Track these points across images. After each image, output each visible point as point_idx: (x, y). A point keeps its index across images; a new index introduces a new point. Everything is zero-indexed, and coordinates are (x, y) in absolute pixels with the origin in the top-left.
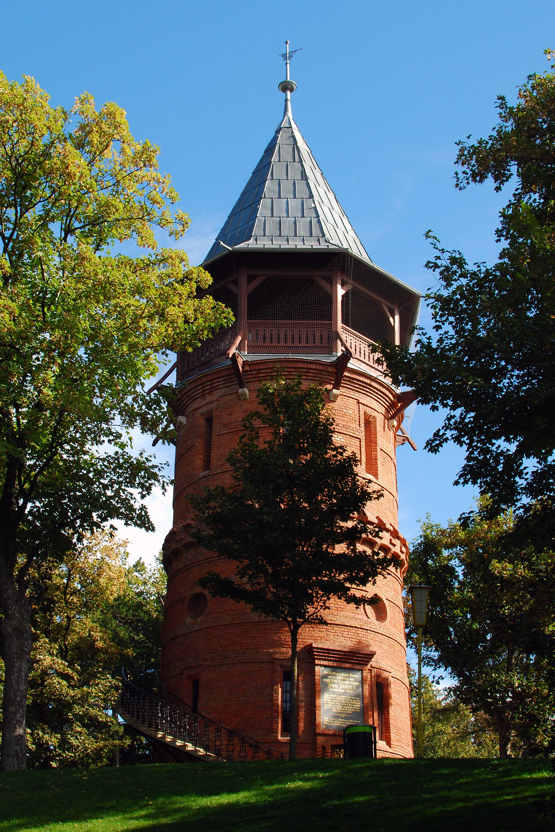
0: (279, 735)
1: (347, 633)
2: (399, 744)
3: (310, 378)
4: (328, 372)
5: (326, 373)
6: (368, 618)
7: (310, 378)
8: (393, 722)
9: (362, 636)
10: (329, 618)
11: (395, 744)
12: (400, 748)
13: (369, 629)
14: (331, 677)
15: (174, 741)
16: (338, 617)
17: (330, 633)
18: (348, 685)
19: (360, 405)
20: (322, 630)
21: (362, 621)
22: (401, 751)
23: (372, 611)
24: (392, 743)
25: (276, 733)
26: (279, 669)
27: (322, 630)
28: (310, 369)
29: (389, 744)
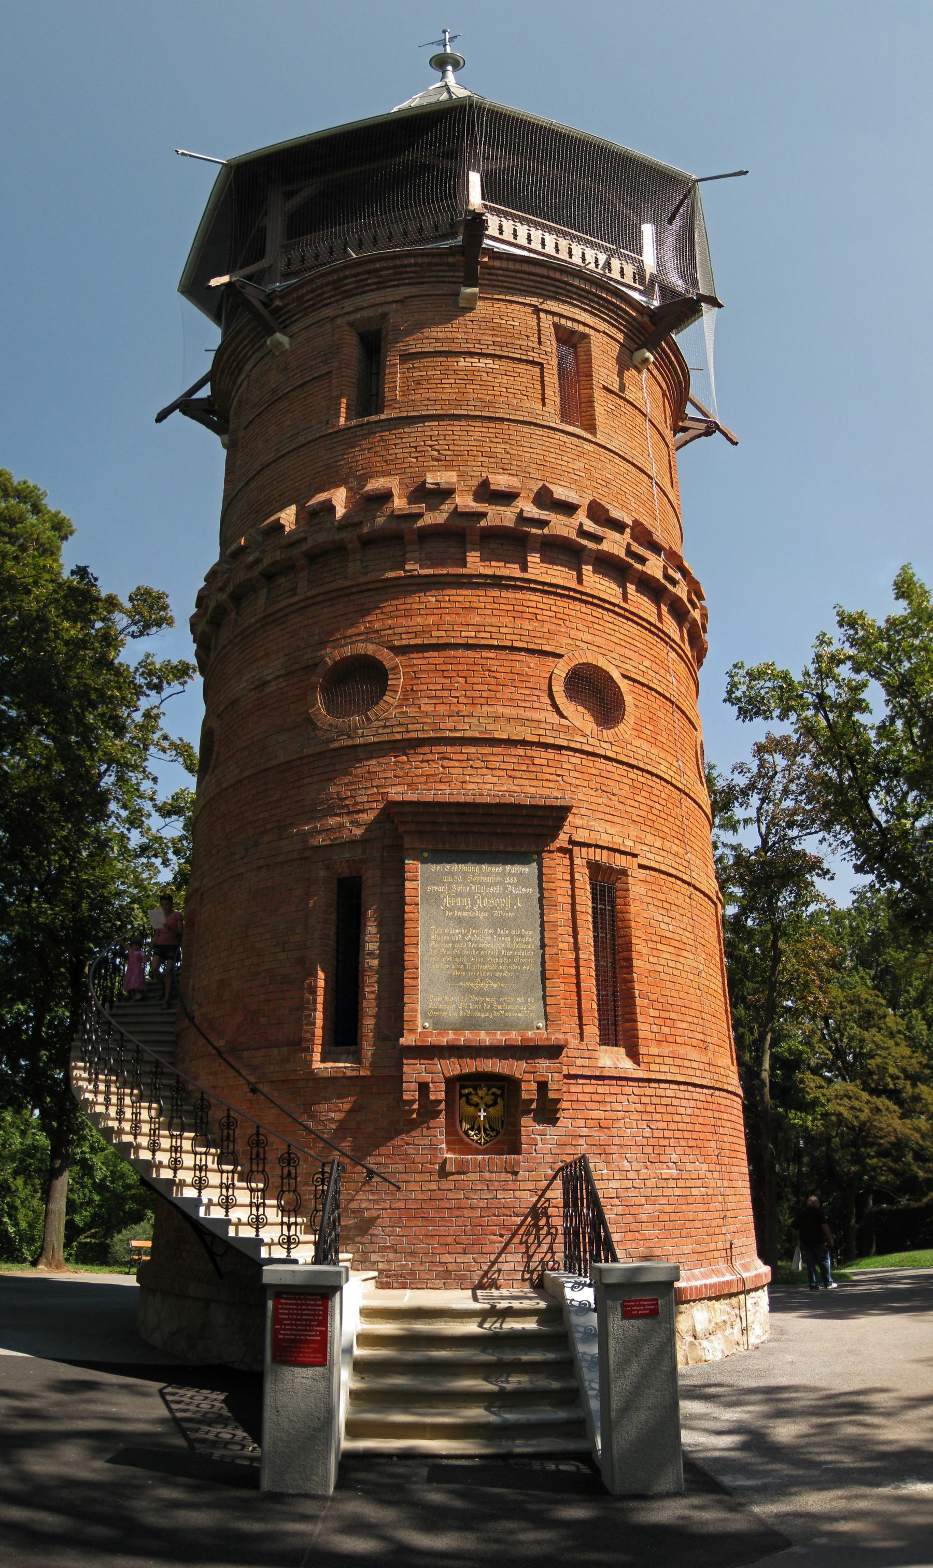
0: (317, 1056)
1: (500, 758)
2: (666, 1050)
3: (407, 281)
4: (448, 264)
5: (446, 268)
6: (562, 716)
7: (407, 281)
8: (645, 988)
9: (545, 762)
10: (450, 724)
11: (654, 1050)
12: (667, 1060)
13: (565, 743)
14: (450, 878)
15: (68, 1017)
16: (474, 720)
17: (452, 764)
18: (499, 896)
19: (542, 315)
20: (430, 757)
21: (543, 725)
22: (675, 1069)
23: (580, 708)
24: (642, 1050)
25: (309, 1051)
26: (322, 873)
27: (430, 757)
28: (405, 266)
29: (634, 1055)
